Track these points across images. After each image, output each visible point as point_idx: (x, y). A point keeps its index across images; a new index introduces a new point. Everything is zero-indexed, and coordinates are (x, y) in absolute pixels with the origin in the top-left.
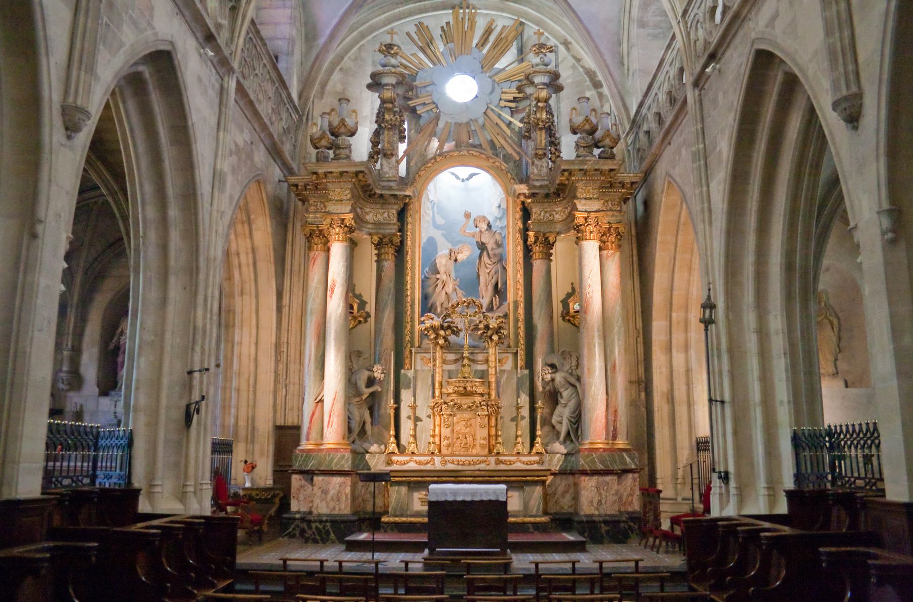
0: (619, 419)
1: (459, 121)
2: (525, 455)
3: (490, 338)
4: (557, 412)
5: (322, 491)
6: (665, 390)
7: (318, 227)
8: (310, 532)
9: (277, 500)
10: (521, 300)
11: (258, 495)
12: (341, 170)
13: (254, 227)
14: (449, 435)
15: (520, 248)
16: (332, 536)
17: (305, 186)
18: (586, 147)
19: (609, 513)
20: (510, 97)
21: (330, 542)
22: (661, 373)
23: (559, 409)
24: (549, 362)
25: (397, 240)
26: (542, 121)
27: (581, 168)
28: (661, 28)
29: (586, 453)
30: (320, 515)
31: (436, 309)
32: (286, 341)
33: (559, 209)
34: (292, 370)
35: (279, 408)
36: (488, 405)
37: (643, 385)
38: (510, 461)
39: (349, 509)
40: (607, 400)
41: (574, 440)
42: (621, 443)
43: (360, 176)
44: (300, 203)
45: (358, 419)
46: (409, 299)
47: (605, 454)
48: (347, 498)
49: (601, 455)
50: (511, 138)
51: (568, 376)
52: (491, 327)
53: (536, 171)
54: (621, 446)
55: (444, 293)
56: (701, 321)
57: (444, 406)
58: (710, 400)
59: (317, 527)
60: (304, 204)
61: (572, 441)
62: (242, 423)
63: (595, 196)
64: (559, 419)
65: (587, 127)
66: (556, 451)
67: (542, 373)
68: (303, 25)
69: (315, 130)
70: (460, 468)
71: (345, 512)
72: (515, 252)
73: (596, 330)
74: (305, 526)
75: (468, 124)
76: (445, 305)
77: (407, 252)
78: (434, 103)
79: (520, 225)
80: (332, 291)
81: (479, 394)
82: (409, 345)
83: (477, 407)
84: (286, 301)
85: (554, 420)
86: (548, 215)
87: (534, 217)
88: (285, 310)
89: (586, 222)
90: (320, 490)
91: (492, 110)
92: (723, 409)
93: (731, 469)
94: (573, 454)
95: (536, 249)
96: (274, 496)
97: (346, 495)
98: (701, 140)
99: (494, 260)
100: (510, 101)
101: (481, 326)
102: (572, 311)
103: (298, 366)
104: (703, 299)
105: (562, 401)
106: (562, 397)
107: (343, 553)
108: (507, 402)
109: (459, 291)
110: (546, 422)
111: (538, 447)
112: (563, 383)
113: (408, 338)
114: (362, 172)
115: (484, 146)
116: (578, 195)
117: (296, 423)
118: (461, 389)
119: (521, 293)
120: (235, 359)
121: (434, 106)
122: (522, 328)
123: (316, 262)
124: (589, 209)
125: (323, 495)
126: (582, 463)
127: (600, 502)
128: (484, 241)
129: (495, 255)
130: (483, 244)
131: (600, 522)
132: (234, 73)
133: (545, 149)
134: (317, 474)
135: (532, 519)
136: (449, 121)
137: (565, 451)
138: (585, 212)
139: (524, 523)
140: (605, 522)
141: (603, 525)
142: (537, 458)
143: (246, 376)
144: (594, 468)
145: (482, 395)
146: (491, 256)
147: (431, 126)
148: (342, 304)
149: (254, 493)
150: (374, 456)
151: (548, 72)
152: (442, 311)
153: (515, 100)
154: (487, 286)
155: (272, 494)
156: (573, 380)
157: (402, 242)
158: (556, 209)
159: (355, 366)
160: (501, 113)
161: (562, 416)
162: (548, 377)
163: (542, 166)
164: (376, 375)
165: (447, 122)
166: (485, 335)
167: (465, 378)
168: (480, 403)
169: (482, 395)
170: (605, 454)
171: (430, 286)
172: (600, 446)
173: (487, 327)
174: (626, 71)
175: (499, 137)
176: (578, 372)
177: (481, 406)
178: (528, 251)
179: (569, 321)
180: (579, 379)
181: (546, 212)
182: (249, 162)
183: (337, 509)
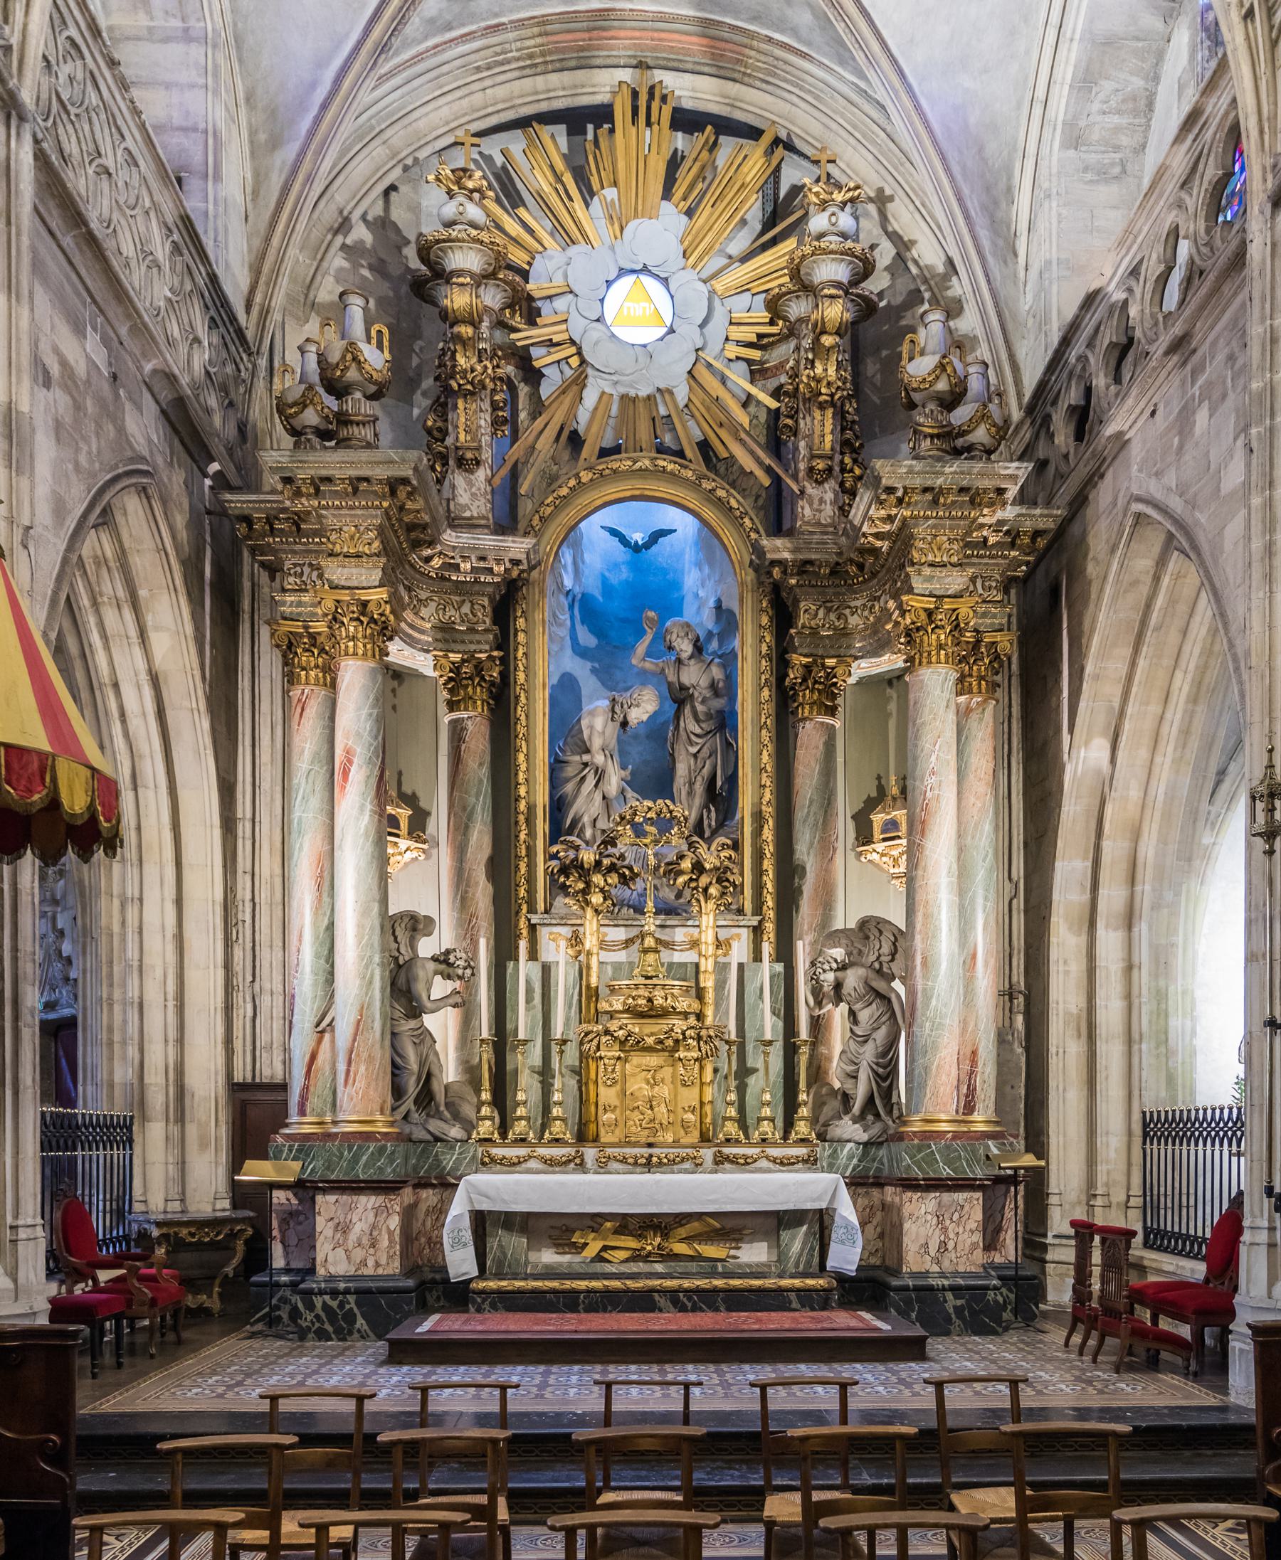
0: (980, 1069)
1: (632, 393)
2: (775, 1145)
3: (706, 890)
5: (336, 1229)
7: (306, 628)
8: (310, 1317)
9: (240, 1246)
11: (193, 1235)
12: (353, 473)
13: (149, 620)
14: (615, 1101)
16: (361, 1322)
17: (269, 521)
18: (938, 436)
19: (961, 1269)
21: (356, 1335)
22: (1067, 973)
26: (829, 384)
27: (929, 483)
28: (1117, 148)
29: (916, 1141)
30: (331, 1278)
31: (582, 830)
32: (248, 896)
33: (858, 603)
34: (266, 964)
35: (238, 1044)
36: (699, 1038)
37: (1021, 999)
38: (746, 1157)
39: (397, 1263)
41: (882, 1113)
43: (402, 492)
44: (264, 577)
45: (414, 1066)
46: (522, 806)
48: (391, 1241)
49: (948, 1147)
51: (872, 975)
52: (707, 866)
53: (807, 512)
54: (981, 1128)
55: (598, 797)
57: (604, 1039)
59: (325, 1305)
60: (273, 579)
61: (877, 1116)
62: (155, 1079)
63: (954, 559)
65: (942, 385)
66: (846, 1136)
68: (241, 102)
69: (288, 385)
71: (389, 1271)
73: (944, 872)
74: (297, 1300)
76: (602, 824)
77: (517, 697)
78: (573, 342)
80: (346, 773)
81: (680, 1013)
82: (524, 907)
83: (677, 1041)
84: (243, 808)
88: (243, 829)
89: (931, 622)
90: (331, 1224)
91: (709, 366)
94: (881, 1143)
96: (233, 1236)
97: (391, 1233)
100: (750, 345)
101: (686, 864)
103: (280, 954)
107: (382, 1370)
109: (630, 794)
111: (802, 1128)
112: (862, 990)
113: (522, 893)
114: (405, 481)
115: (689, 453)
116: (916, 555)
117: (279, 1078)
118: (642, 1002)
120: (131, 937)
121: (573, 350)
122: (771, 873)
123: (307, 711)
124: (936, 587)
125: (338, 1235)
127: (943, 1246)
130: (683, 688)
131: (944, 1289)
132: (22, 119)
133: (831, 458)
134: (325, 1191)
135: (797, 1282)
136: (608, 390)
137: (864, 1137)
139: (781, 1290)
140: (954, 1289)
141: (949, 1295)
142: (802, 1151)
143: (159, 972)
144: (932, 1175)
145: (685, 1015)
146: (701, 717)
147: (567, 400)
148: (369, 807)
149: (184, 1232)
150: (453, 1148)
151: (850, 253)
152: (594, 836)
153: (760, 343)
155: (226, 1231)
157: (505, 675)
158: (853, 604)
159: (403, 950)
160: (727, 373)
163: (821, 501)
165: (603, 393)
166: (693, 885)
167: (647, 978)
168: (683, 1033)
169: (685, 1015)
171: (568, 780)
172: (944, 1127)
173: (698, 867)
174: (1022, 273)
175: (723, 434)
177: (685, 1038)
182: (110, 429)
183: (371, 1262)
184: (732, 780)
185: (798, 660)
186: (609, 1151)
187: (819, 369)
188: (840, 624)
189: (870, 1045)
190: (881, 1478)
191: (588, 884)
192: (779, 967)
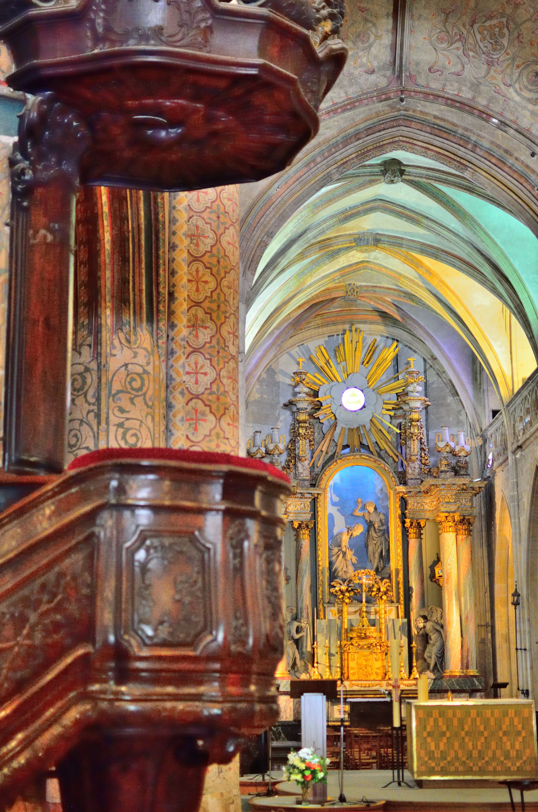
2: (405, 680)
3: (381, 597)
4: (427, 650)
6: (504, 633)
10: (401, 568)
15: (399, 530)
20: (390, 407)
22: (501, 621)
23: (429, 647)
24: (422, 614)
25: (311, 525)
36: (380, 646)
40: (462, 642)
42: (473, 671)
47: (460, 679)
50: (391, 443)
51: (435, 624)
56: (513, 604)
57: (351, 646)
58: (517, 649)
61: (438, 671)
64: (429, 655)
67: (417, 623)
70: (362, 689)
72: (396, 532)
75: (358, 428)
79: (399, 512)
85: (426, 655)
86: (419, 505)
87: (409, 507)
92: (526, 654)
93: (530, 689)
95: (411, 531)
97: (290, 708)
98: (516, 489)
99: (379, 534)
101: (375, 589)
102: (437, 575)
104: (514, 591)
105: (431, 642)
106: (431, 639)
108: (393, 644)
110: (421, 657)
111: (415, 673)
112: (431, 629)
119: (401, 563)
124: (448, 510)
126: (445, 684)
128: (371, 520)
129: (380, 530)
130: (371, 522)
137: (434, 677)
138: (446, 512)
154: (374, 554)
156: (438, 628)
161: (432, 652)
162: (421, 625)
164: (302, 625)
170: (460, 679)
172: (458, 674)
176: (442, 621)
178: (405, 532)
179: (435, 581)
180: (442, 627)
181: (418, 503)
184: (388, 551)
185: (408, 520)
186: (353, 682)
187: (412, 430)
188: (422, 508)
189: (435, 647)
190: (115, 46)
191: (344, 595)
192: (406, 620)
